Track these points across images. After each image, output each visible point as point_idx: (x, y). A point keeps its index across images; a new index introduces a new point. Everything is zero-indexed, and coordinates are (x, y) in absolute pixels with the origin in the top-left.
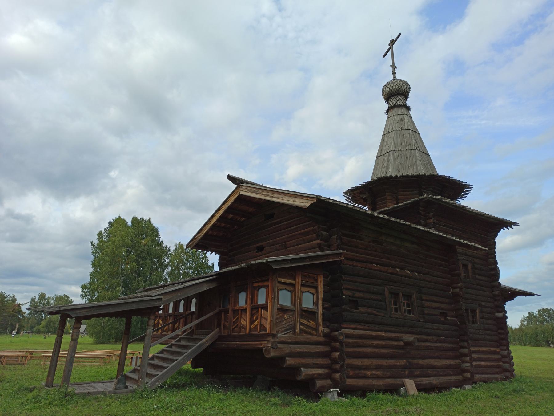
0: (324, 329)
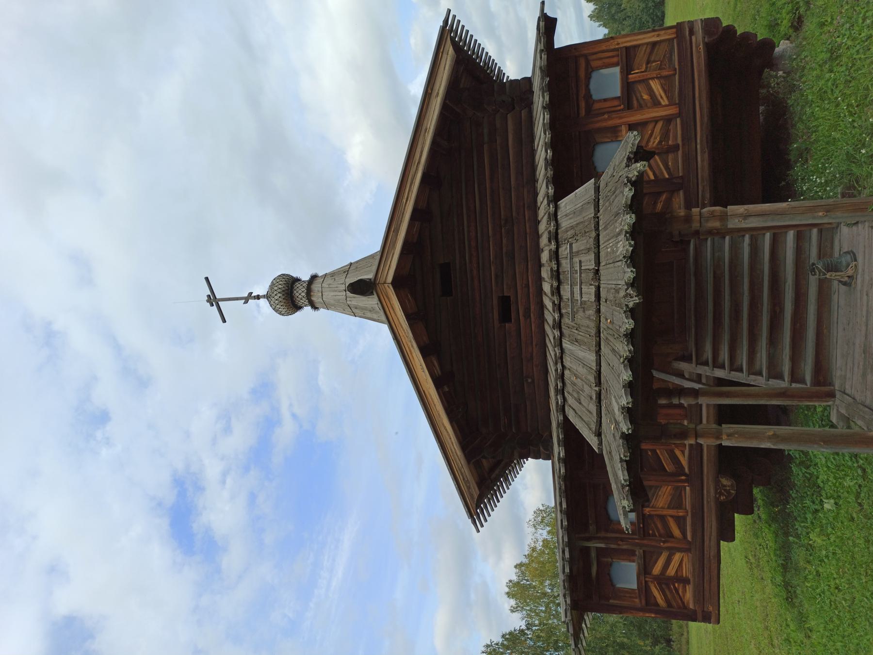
0: (619, 49)
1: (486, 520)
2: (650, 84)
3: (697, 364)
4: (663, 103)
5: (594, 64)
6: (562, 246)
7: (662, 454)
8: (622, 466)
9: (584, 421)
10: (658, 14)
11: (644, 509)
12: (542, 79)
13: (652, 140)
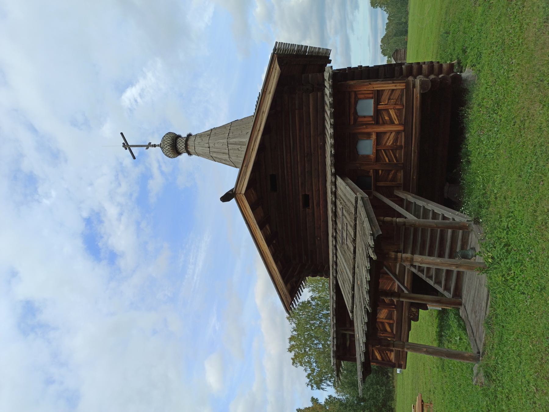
2: (389, 111)
13: (388, 142)
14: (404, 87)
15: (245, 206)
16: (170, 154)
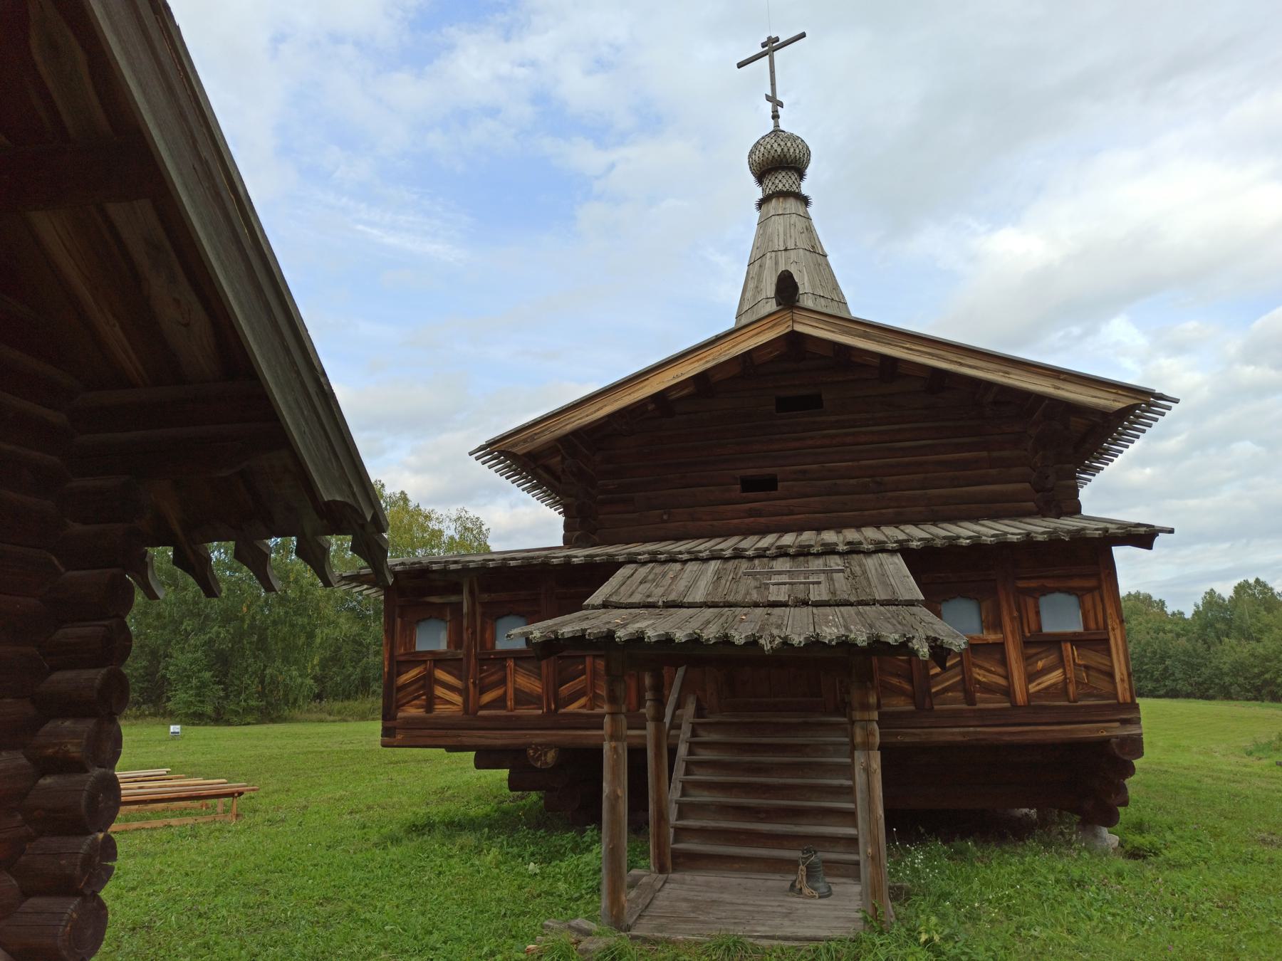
1: (484, 463)
2: (1058, 669)
3: (691, 743)
4: (1030, 686)
5: (1088, 599)
6: (842, 559)
7: (580, 681)
8: (577, 630)
9: (619, 588)
10: (1211, 691)
11: (513, 660)
12: (1069, 532)
13: (982, 672)
14: (1121, 700)
15: (761, 334)
16: (761, 154)
